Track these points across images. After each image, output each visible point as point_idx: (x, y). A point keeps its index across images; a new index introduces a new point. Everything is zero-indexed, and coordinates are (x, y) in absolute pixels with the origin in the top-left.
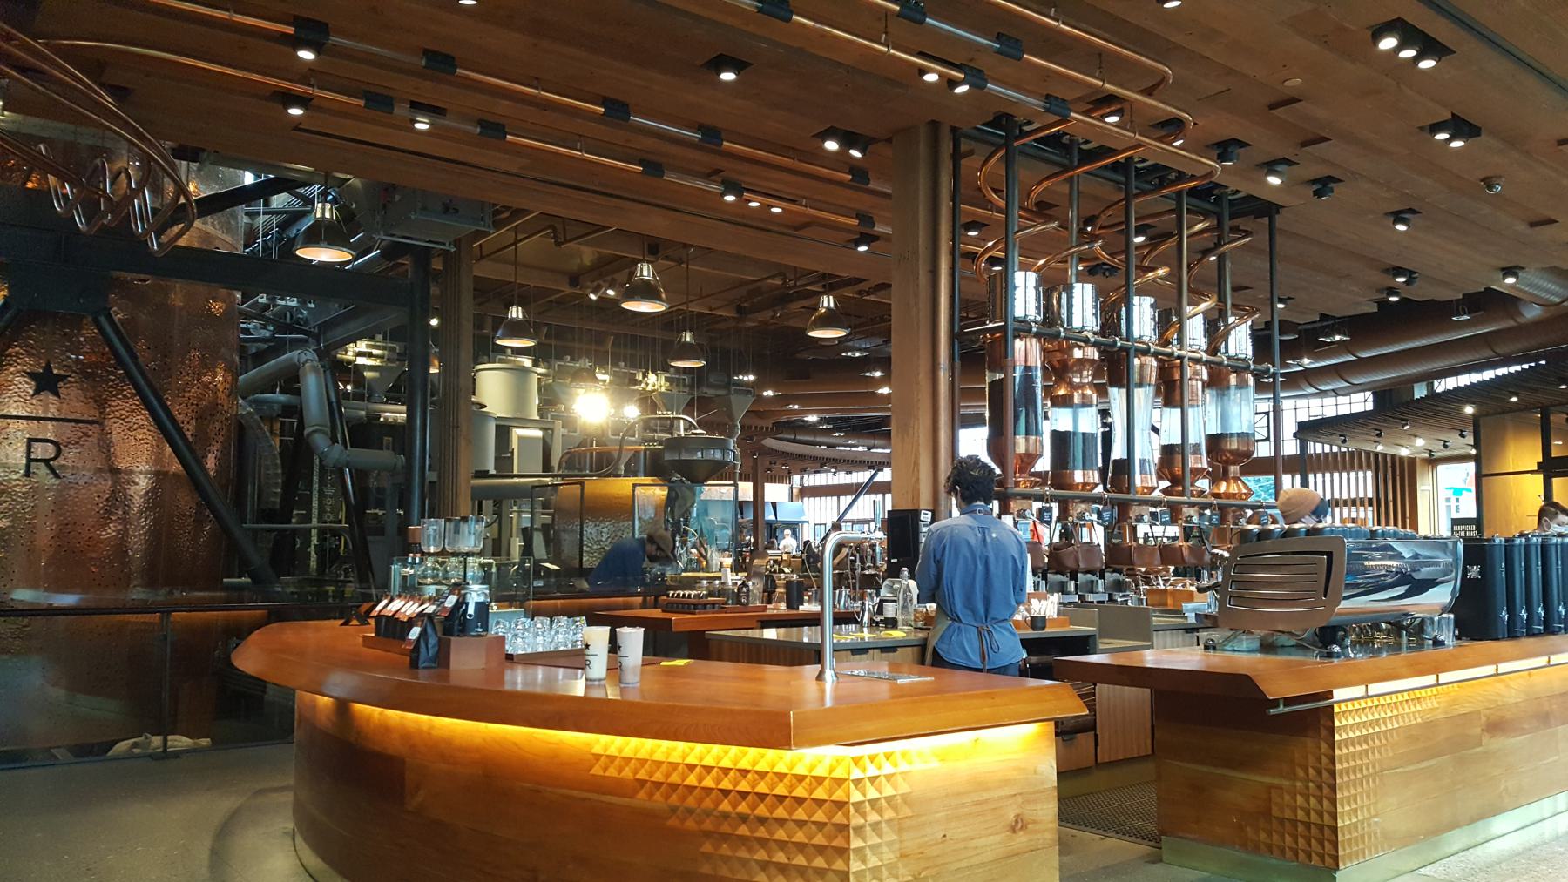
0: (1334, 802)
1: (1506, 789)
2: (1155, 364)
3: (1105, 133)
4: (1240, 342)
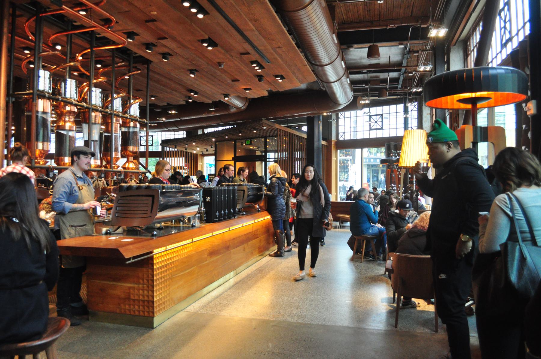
0: (153, 291)
2: (101, 115)
3: (79, 18)
4: (135, 110)
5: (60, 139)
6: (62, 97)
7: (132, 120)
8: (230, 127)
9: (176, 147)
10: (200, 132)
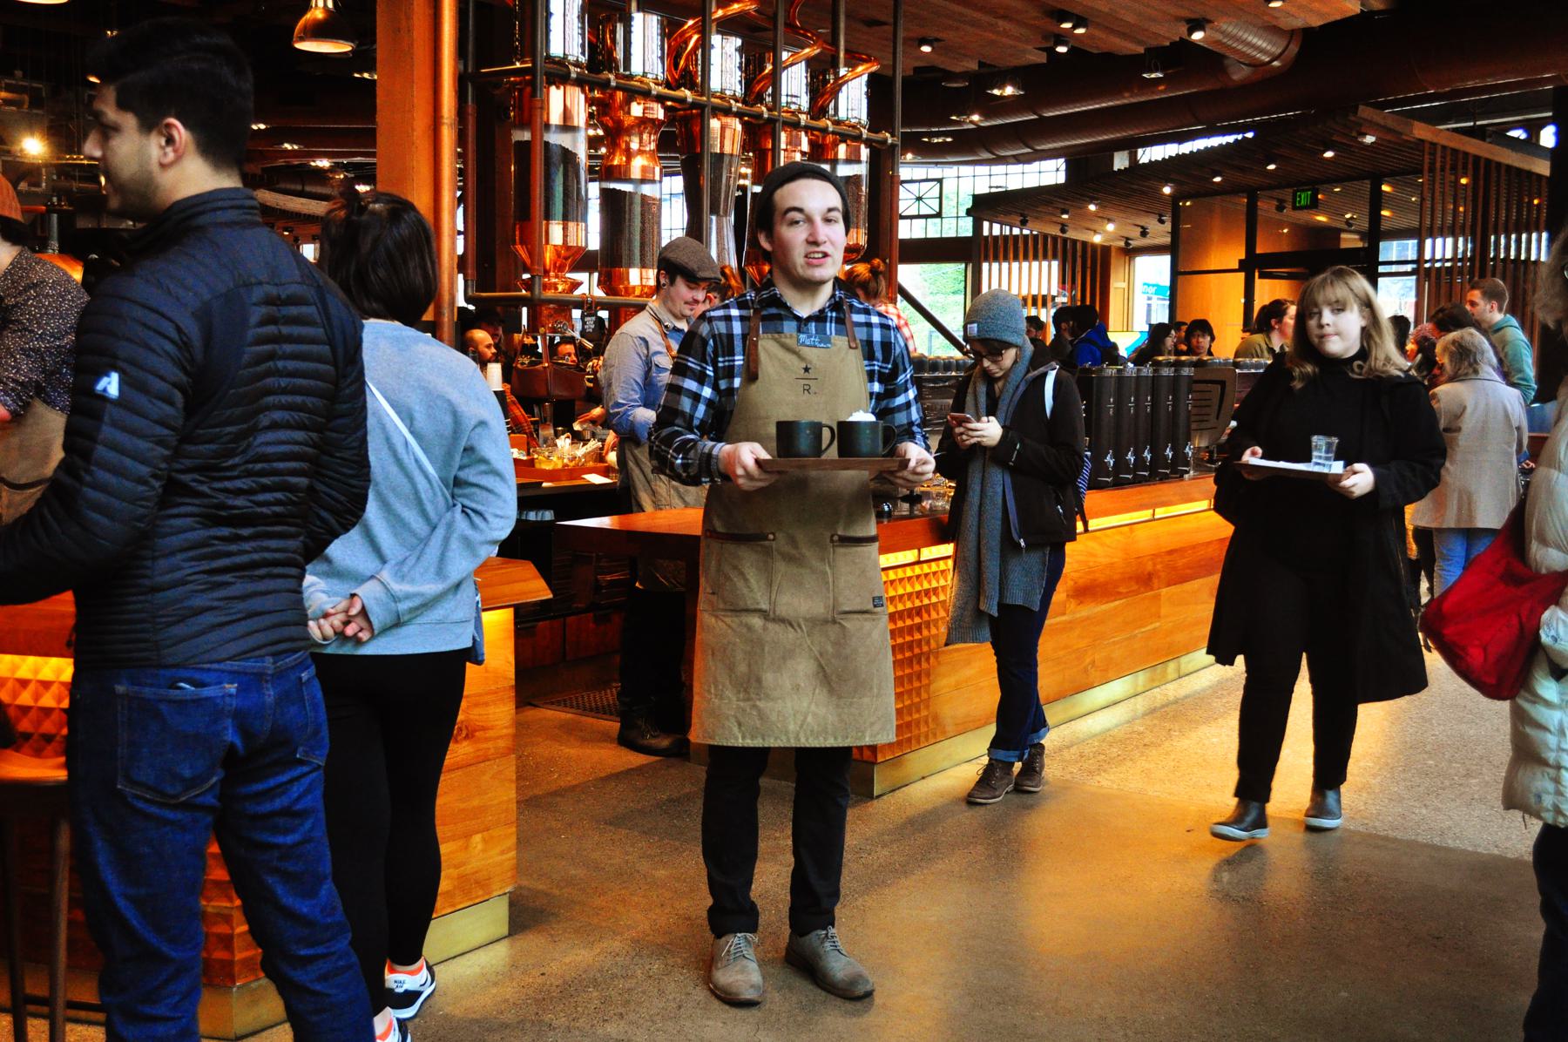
1: (1093, 663)
2: (739, 127)
4: (853, 101)
5: (614, 205)
6: (617, 77)
7: (844, 138)
8: (1230, 139)
9: (1024, 223)
10: (1120, 161)
